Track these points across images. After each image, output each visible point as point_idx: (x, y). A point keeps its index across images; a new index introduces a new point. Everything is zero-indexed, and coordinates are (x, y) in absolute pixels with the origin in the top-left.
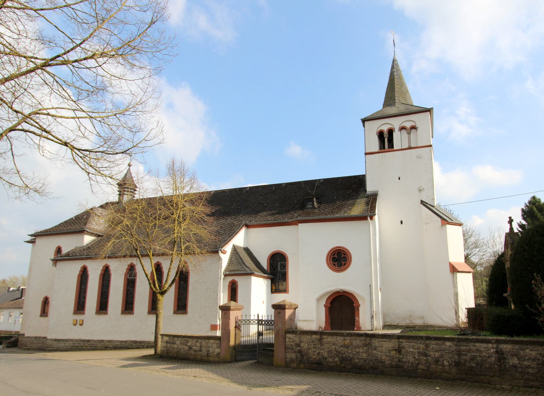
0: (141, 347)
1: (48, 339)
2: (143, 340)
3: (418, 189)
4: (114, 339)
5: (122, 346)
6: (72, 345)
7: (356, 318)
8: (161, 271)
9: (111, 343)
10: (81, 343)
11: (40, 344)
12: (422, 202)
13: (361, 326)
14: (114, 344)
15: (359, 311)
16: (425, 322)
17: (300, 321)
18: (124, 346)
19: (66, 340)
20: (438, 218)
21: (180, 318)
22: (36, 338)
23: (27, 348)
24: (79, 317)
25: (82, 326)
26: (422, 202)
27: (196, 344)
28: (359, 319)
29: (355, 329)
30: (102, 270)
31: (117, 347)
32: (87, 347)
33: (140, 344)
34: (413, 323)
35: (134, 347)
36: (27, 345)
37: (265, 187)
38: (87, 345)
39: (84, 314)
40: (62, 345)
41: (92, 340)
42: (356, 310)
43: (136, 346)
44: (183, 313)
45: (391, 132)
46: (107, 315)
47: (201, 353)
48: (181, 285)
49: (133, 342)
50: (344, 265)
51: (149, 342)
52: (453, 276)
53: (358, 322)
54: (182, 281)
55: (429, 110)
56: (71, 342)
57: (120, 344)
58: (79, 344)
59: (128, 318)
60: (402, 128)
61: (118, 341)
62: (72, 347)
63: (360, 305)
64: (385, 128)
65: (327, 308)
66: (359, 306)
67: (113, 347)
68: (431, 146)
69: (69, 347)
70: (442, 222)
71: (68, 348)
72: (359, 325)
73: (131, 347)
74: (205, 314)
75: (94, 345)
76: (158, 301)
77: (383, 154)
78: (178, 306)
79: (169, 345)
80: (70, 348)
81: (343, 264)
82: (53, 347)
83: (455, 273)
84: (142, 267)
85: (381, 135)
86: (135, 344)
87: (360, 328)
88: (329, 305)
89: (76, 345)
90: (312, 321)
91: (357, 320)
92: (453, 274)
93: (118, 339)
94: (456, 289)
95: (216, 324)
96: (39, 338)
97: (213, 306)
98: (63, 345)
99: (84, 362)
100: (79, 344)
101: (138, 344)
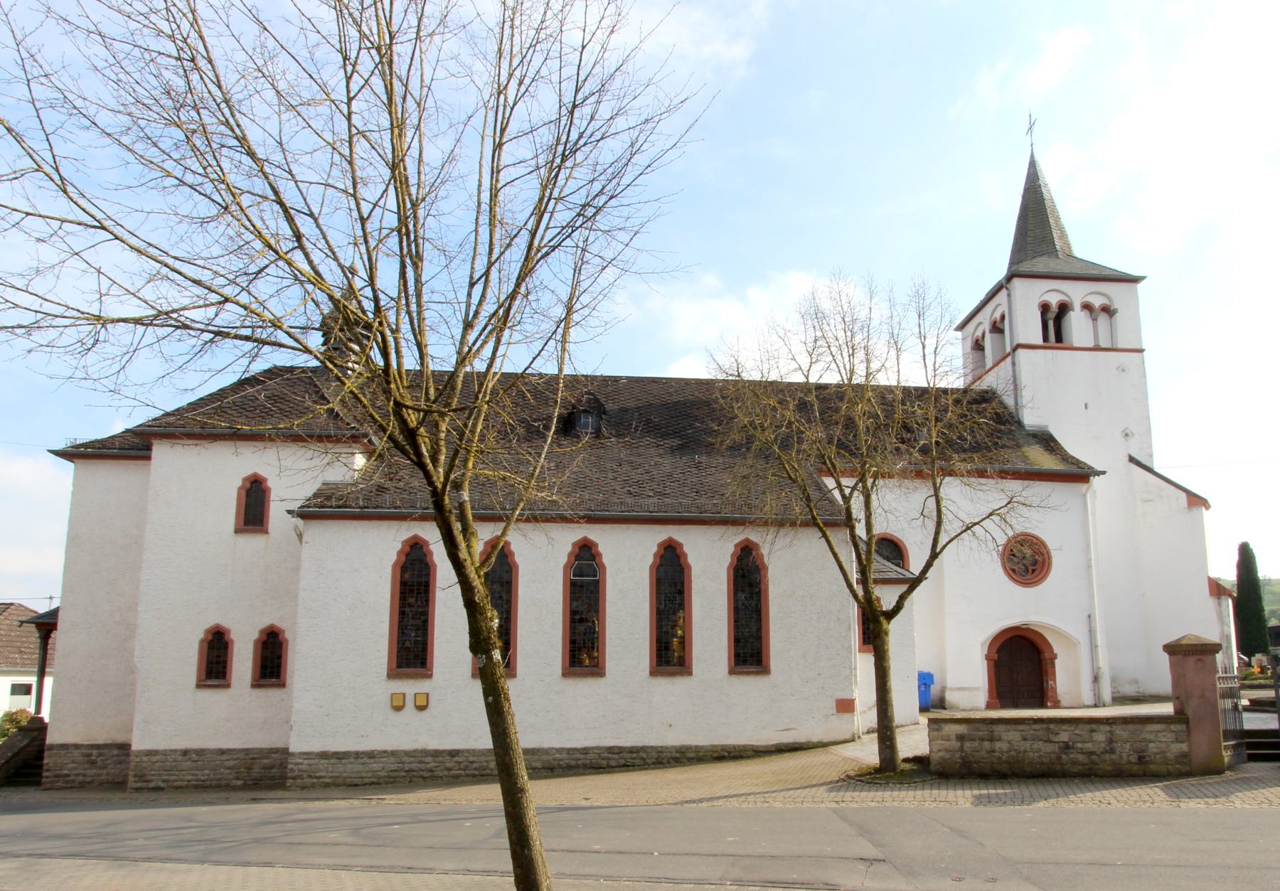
0: (637, 762)
1: (293, 754)
2: (640, 744)
3: (1123, 431)
4: (546, 745)
5: (573, 763)
6: (394, 767)
7: (1050, 682)
8: (509, 565)
9: (536, 757)
10: (429, 759)
11: (206, 772)
12: (1132, 459)
13: (1059, 698)
14: (545, 758)
15: (1054, 667)
16: (1141, 690)
17: (952, 689)
18: (580, 762)
19: (371, 755)
20: (1180, 491)
21: (671, 688)
22: (185, 753)
23: (152, 785)
24: (410, 687)
25: (424, 712)
26: (1132, 459)
27: (1092, 737)
28: (1055, 684)
29: (1049, 704)
30: (399, 553)
31: (559, 765)
32: (449, 769)
33: (635, 755)
34: (1119, 692)
35: (613, 763)
36: (149, 778)
37: (642, 381)
38: (448, 765)
39: (430, 676)
40: (350, 768)
41: (468, 751)
42: (1049, 666)
43: (622, 762)
44: (757, 673)
45: (1064, 308)
46: (515, 680)
47: (1113, 757)
48: (740, 603)
49: (611, 750)
50: (1032, 573)
51: (662, 747)
52: (1220, 604)
53: (1054, 690)
54: (743, 591)
55: (1134, 280)
56: (392, 760)
57: (568, 759)
58: (421, 762)
59: (585, 687)
60: (1087, 307)
61: (560, 750)
62: (396, 774)
63: (1056, 655)
64: (1054, 300)
65: (992, 663)
66: (1055, 657)
67: (543, 768)
68: (1141, 351)
69: (383, 774)
70: (1188, 499)
71: (379, 778)
72: (1056, 697)
73: (604, 763)
74: (819, 675)
75: (475, 765)
76: (884, 636)
77: (1054, 351)
78: (737, 655)
79: (968, 745)
80: (385, 777)
81: (1030, 571)
82: (320, 777)
83: (1223, 597)
84: (949, 546)
85: (1045, 308)
86: (616, 756)
87: (1058, 702)
88: (996, 657)
89: (407, 767)
90: (976, 689)
91: (1052, 688)
92: (1219, 598)
93: (558, 746)
94: (1225, 627)
95: (849, 697)
96: (201, 752)
97: (838, 654)
98: (358, 767)
99: (734, 803)
100: (421, 762)
101: (627, 755)
